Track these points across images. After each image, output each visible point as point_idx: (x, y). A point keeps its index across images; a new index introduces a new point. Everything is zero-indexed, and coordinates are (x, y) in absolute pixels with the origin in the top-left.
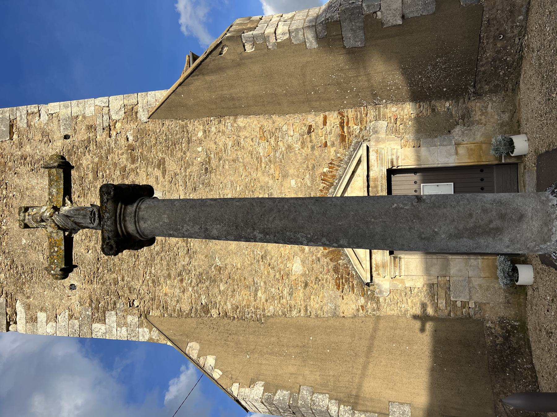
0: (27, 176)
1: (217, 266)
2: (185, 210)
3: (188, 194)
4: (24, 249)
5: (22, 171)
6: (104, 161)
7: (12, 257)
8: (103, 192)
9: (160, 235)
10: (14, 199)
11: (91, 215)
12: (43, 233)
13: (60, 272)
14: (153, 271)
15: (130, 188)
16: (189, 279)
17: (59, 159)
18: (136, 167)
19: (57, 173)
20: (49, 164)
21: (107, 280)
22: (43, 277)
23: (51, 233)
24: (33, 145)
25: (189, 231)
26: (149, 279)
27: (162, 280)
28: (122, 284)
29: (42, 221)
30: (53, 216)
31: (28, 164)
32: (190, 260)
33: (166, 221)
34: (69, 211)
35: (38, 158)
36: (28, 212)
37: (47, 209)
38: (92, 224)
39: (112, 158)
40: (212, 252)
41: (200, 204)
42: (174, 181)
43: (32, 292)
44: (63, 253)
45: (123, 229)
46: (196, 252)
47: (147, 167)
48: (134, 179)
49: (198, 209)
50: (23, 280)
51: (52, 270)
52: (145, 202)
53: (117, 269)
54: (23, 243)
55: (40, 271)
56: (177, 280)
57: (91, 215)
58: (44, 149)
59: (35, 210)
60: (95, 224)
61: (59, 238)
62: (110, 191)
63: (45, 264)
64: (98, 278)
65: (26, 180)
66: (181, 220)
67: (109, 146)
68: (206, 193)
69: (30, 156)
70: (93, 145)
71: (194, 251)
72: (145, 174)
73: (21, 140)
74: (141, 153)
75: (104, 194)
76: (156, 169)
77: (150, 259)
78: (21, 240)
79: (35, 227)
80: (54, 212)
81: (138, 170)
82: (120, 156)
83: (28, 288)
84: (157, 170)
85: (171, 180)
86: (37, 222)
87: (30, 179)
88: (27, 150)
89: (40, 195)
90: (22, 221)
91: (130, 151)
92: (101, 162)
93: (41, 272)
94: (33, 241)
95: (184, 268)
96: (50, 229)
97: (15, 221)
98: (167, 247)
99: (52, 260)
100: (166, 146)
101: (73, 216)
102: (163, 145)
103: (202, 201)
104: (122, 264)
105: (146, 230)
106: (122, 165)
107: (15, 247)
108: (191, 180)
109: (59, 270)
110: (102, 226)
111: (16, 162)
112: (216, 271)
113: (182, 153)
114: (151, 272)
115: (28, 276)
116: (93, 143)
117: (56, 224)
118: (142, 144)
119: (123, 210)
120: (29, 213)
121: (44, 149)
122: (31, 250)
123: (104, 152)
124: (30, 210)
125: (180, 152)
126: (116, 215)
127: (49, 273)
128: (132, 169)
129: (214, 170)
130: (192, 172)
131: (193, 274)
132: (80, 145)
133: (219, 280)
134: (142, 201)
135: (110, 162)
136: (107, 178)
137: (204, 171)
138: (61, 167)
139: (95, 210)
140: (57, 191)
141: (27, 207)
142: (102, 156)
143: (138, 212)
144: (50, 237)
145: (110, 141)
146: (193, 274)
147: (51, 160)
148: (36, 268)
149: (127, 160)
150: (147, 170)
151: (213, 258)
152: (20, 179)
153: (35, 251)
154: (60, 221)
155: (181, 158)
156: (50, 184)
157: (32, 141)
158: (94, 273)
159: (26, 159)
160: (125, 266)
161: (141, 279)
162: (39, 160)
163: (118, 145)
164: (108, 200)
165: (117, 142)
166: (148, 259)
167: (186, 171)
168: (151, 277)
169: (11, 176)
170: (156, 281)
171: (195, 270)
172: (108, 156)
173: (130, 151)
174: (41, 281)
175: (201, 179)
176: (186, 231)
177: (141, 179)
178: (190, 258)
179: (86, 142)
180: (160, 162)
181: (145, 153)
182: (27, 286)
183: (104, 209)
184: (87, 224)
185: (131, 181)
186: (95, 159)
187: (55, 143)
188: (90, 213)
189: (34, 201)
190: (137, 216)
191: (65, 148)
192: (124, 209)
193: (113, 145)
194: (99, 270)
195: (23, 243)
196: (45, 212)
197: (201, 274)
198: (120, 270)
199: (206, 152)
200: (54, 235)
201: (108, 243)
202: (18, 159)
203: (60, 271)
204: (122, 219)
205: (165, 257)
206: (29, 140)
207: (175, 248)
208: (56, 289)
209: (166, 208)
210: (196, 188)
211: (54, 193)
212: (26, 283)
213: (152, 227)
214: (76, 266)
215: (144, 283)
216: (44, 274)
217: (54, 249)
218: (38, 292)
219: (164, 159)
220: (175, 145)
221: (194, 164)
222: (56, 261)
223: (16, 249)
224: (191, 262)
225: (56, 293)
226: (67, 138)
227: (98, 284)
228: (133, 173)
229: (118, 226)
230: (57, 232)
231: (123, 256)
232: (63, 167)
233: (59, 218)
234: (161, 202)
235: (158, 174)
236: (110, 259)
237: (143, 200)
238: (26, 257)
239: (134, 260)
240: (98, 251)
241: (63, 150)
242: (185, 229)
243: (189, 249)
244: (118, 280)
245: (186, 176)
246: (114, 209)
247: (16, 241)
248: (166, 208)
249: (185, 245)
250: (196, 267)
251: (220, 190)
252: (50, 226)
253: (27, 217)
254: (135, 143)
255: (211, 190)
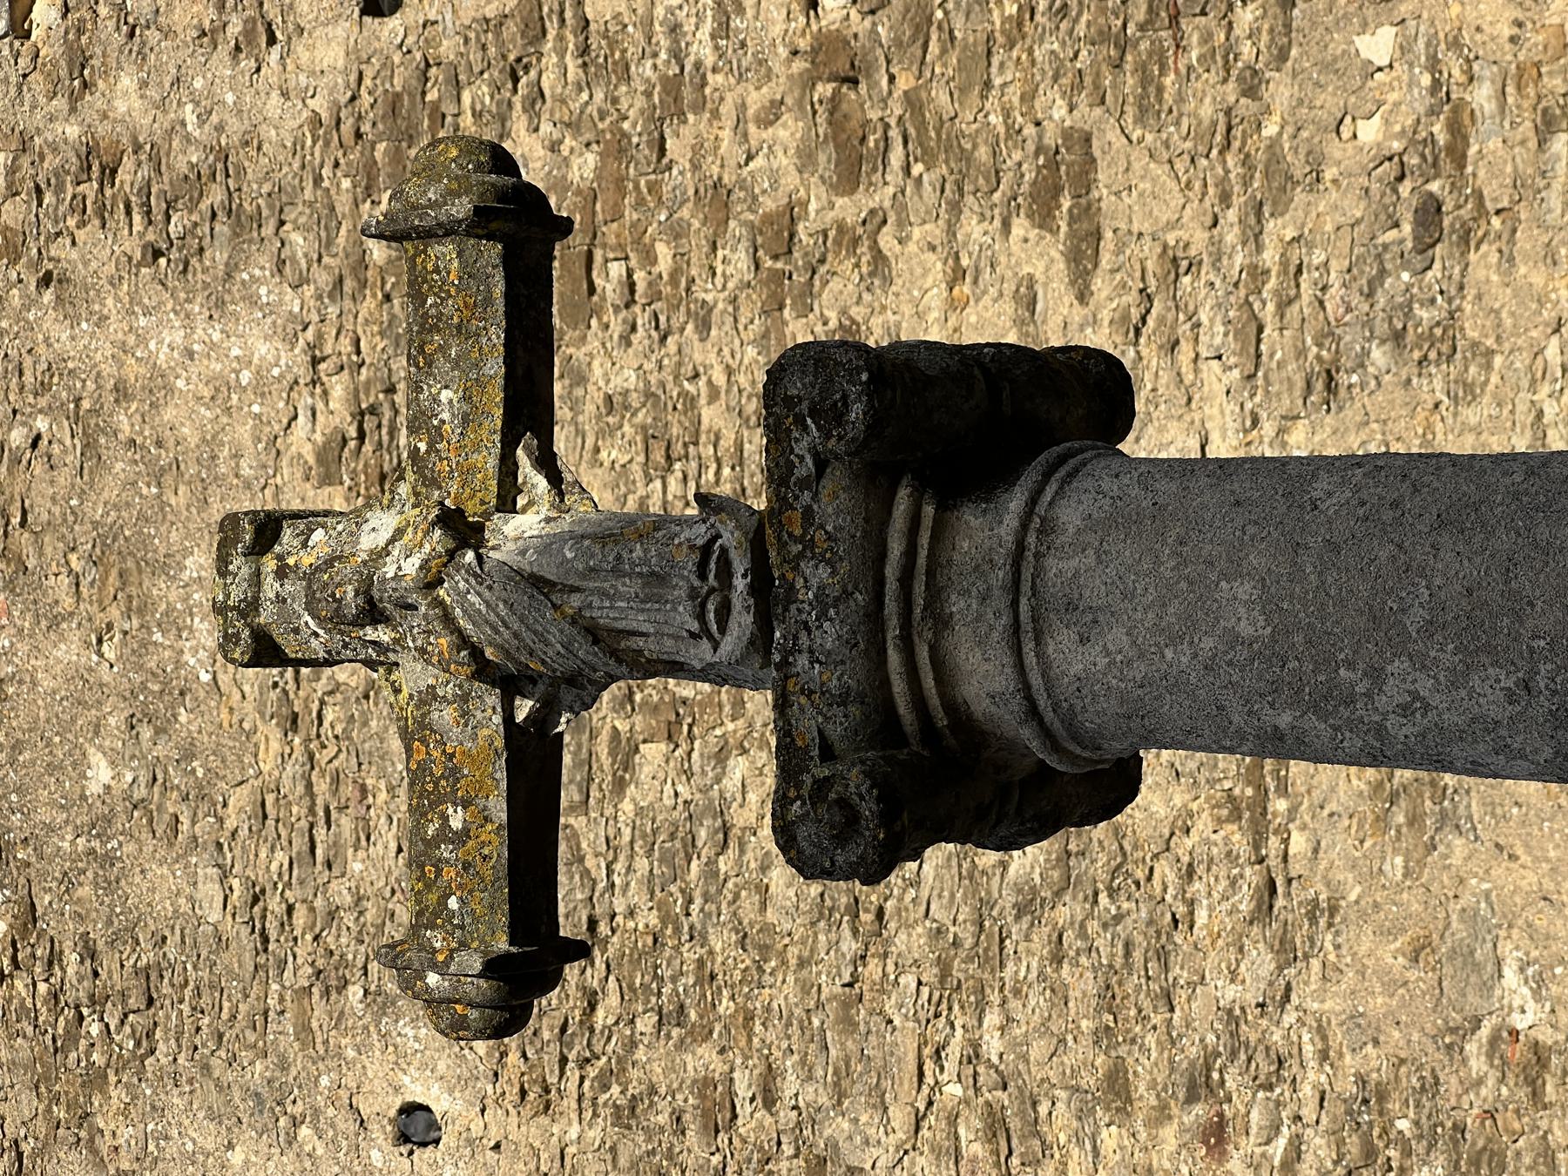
0: (118, 299)
1: (1514, 1034)
2: (1400, 547)
3: (1268, 428)
4: (100, 825)
5: (86, 263)
6: (638, 174)
7: (22, 881)
8: (790, 402)
9: (1191, 740)
10: (38, 468)
11: (703, 576)
12: (224, 715)
13: (483, 983)
14: (993, 1045)
15: (976, 372)
16: (1276, 1128)
17: (479, 167)
18: (872, 212)
19: (468, 273)
20: (414, 207)
21: (653, 1090)
22: (221, 1036)
23: (422, 703)
24: (159, 69)
25: (1426, 707)
26: (966, 1101)
27: (1060, 1120)
28: (761, 1126)
29: (373, 613)
30: (441, 582)
31: (128, 213)
32: (1280, 968)
33: (1245, 629)
34: (547, 546)
35: (192, 166)
36: (277, 548)
37: (399, 533)
38: (705, 644)
39: (697, 150)
40: (1466, 914)
41: (1516, 496)
42: (1161, 320)
43: (151, 1148)
44: (495, 846)
45: (929, 682)
46: (1333, 910)
47: (956, 208)
48: (854, 311)
49: (1504, 541)
50: (95, 1057)
51: (434, 966)
52: (1089, 483)
53: (725, 1006)
54: (94, 788)
55: (205, 992)
56: (1183, 1130)
57: (703, 576)
58: (230, 98)
59: (319, 535)
60: (732, 643)
61: (474, 737)
62: (845, 397)
63: (233, 946)
64: (592, 1072)
65: (115, 326)
66: (1362, 622)
67: (677, 55)
68: (1421, 414)
69: (137, 148)
70: (562, 54)
71: (1316, 901)
72: (937, 268)
73: (80, 31)
74: (913, 102)
75: (800, 422)
76: (1020, 226)
77: (969, 943)
78: (80, 765)
79: (322, 654)
80: (451, 554)
81: (886, 240)
82: (752, 128)
83: (125, 1112)
84: (1033, 234)
85: (1135, 314)
86: (336, 620)
87: (143, 321)
88: (121, 107)
89: (204, 440)
90: (243, 614)
91: (824, 89)
92: (620, 182)
93: (205, 1001)
94: (160, 777)
95: (1235, 1035)
96: (414, 675)
97: (44, 623)
98: (1102, 858)
99: (432, 898)
100: (1102, 37)
101: (573, 581)
102: (1081, 30)
103: (1530, 473)
104: (761, 970)
105: (1095, 696)
106: (769, 204)
107: (44, 815)
108: (1295, 308)
109: (478, 966)
110: (777, 658)
111: (48, 199)
112: (1502, 1080)
113: (1231, 85)
114: (976, 1045)
115: (127, 1029)
116: (560, 38)
117: (463, 641)
118: (917, 28)
119: (924, 540)
120: (280, 558)
121: (230, 98)
122: (145, 835)
123: (640, 102)
124: (287, 535)
125: (1213, 77)
126: (880, 582)
127: (410, 980)
128: (841, 227)
129: (1496, 222)
130: (1311, 246)
131: (1306, 1091)
132: (475, 56)
133: (1527, 1160)
134: (1062, 472)
135: (680, 178)
136: (657, 306)
137: (1407, 228)
138: (494, 226)
139: (730, 537)
140: (467, 398)
141: (268, 514)
142: (624, 135)
143: (1037, 555)
144: (415, 732)
145: (681, 15)
146: (1306, 1091)
147: (430, 181)
148: (179, 968)
149: (806, 159)
150: (951, 232)
151: (1477, 967)
152: (75, 321)
153: (171, 845)
154: (492, 617)
155: (1221, 128)
156: (421, 350)
157: (153, 36)
158: (564, 1029)
159: (114, 171)
160: (783, 992)
161: (904, 1099)
162: (196, 182)
163: (743, 45)
164: (821, 465)
165: (736, 22)
166: (956, 943)
167: (1254, 238)
168: (977, 1090)
169: (17, 302)
170: (1014, 1124)
171: (1324, 1056)
172: (667, 132)
173: (824, 89)
174: (206, 1068)
175: (1381, 300)
176: (1405, 710)
177: (908, 310)
178: (1286, 953)
179: (511, 28)
180: (1053, 164)
181: (944, 98)
182: (118, 1095)
183: (798, 532)
184: (669, 643)
185: (833, 324)
186: (576, 162)
187: (299, 48)
188: (696, 557)
189: (168, 480)
190: (1026, 587)
191: (367, 82)
192: (936, 538)
193: (702, 48)
194: (600, 1013)
195: (94, 788)
196: (385, 552)
197: (1373, 1095)
198: (749, 1018)
199: (1433, 65)
200: (445, 716)
201: (822, 786)
202: (60, 172)
203: (478, 976)
204: (918, 611)
205: (1082, 933)
206: (132, 35)
207: (1165, 870)
208: (305, 1131)
209: (1251, 530)
210: (1343, 379)
211: (446, 416)
212: (112, 1079)
213: (1139, 670)
214: (580, 951)
215: (925, 1132)
216: (225, 1015)
217: (445, 818)
218: (190, 1147)
219: (1087, 139)
220: (1174, 19)
221: (1329, 173)
222: (453, 903)
223: (50, 828)
224: (1288, 988)
225: (308, 1164)
226: (386, 9)
227: (588, 1115)
228: (849, 264)
229: (894, 658)
230: (465, 698)
231: (771, 917)
232: (507, 227)
233: (487, 594)
234: (1203, 481)
235: (1037, 269)
236: (677, 930)
237: (1072, 462)
238: (111, 886)
239: (850, 946)
240: (590, 862)
241: (353, 99)
242: (1393, 693)
243: (1280, 882)
244: (731, 1094)
245: (1258, 274)
246: (866, 534)
247: (51, 768)
248: (1251, 530)
249: (1240, 841)
250: (1337, 1036)
251: (1545, 389)
252: (422, 651)
253: (270, 587)
254: (867, 23)
255: (1466, 392)
